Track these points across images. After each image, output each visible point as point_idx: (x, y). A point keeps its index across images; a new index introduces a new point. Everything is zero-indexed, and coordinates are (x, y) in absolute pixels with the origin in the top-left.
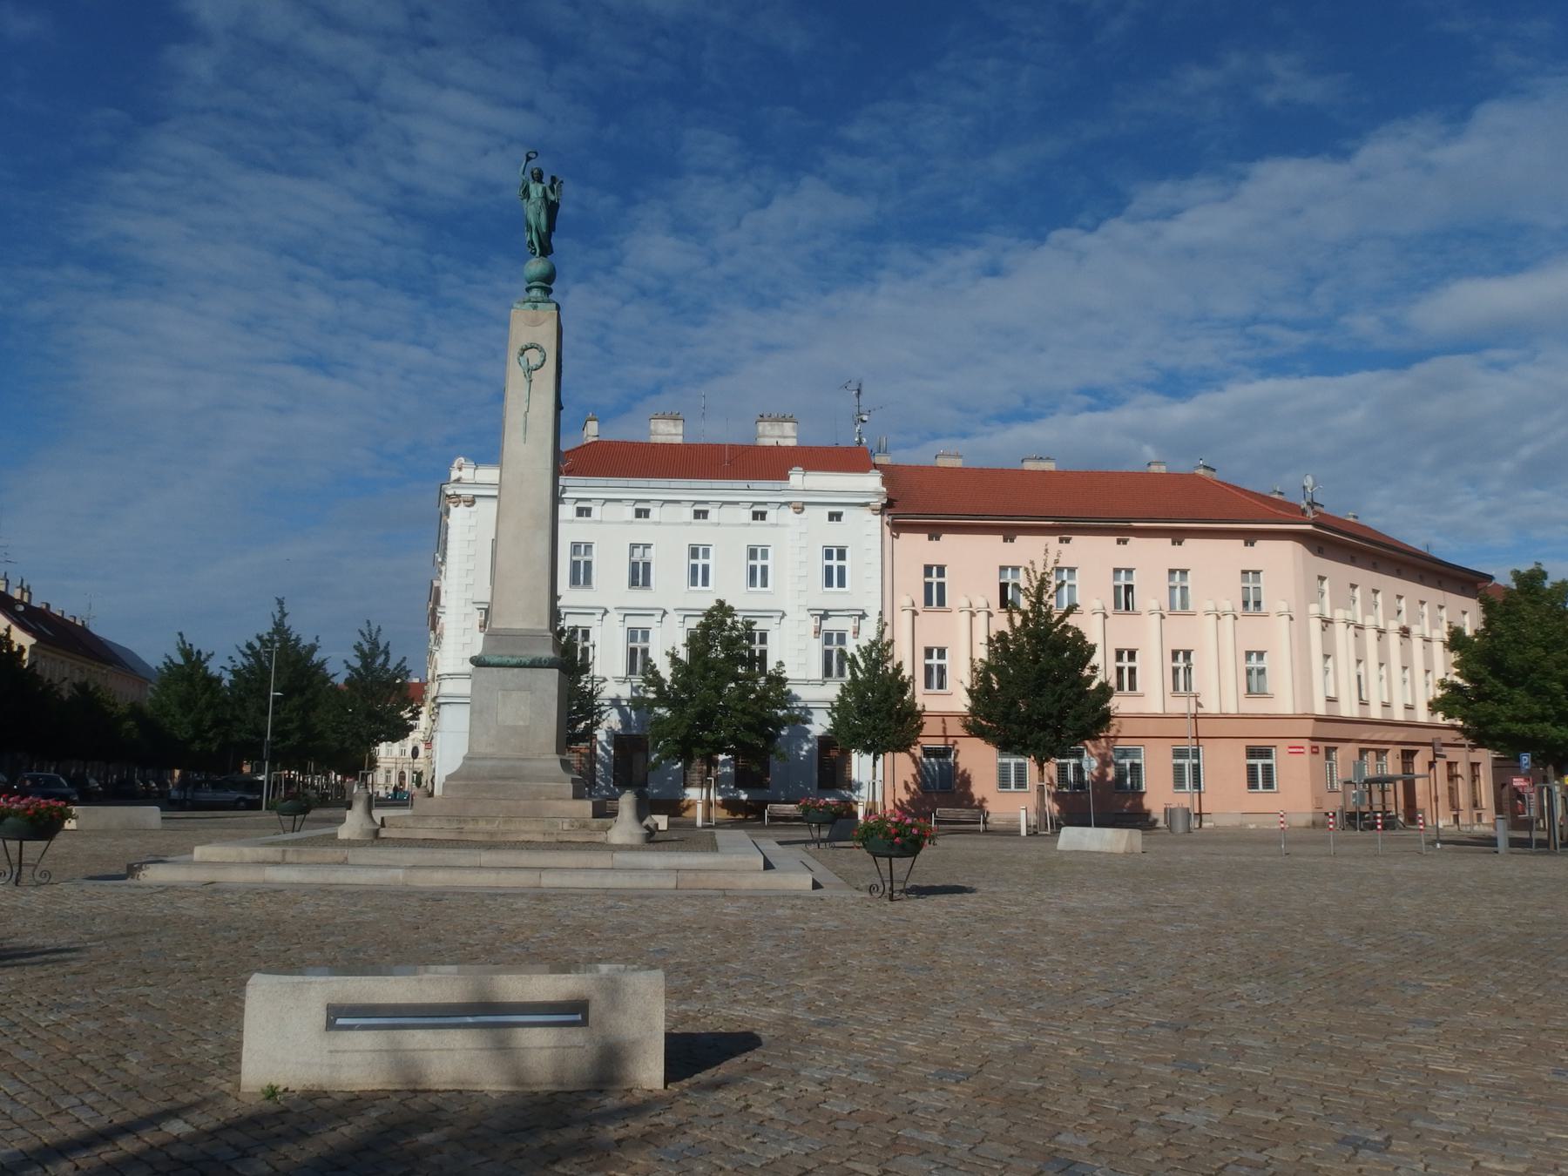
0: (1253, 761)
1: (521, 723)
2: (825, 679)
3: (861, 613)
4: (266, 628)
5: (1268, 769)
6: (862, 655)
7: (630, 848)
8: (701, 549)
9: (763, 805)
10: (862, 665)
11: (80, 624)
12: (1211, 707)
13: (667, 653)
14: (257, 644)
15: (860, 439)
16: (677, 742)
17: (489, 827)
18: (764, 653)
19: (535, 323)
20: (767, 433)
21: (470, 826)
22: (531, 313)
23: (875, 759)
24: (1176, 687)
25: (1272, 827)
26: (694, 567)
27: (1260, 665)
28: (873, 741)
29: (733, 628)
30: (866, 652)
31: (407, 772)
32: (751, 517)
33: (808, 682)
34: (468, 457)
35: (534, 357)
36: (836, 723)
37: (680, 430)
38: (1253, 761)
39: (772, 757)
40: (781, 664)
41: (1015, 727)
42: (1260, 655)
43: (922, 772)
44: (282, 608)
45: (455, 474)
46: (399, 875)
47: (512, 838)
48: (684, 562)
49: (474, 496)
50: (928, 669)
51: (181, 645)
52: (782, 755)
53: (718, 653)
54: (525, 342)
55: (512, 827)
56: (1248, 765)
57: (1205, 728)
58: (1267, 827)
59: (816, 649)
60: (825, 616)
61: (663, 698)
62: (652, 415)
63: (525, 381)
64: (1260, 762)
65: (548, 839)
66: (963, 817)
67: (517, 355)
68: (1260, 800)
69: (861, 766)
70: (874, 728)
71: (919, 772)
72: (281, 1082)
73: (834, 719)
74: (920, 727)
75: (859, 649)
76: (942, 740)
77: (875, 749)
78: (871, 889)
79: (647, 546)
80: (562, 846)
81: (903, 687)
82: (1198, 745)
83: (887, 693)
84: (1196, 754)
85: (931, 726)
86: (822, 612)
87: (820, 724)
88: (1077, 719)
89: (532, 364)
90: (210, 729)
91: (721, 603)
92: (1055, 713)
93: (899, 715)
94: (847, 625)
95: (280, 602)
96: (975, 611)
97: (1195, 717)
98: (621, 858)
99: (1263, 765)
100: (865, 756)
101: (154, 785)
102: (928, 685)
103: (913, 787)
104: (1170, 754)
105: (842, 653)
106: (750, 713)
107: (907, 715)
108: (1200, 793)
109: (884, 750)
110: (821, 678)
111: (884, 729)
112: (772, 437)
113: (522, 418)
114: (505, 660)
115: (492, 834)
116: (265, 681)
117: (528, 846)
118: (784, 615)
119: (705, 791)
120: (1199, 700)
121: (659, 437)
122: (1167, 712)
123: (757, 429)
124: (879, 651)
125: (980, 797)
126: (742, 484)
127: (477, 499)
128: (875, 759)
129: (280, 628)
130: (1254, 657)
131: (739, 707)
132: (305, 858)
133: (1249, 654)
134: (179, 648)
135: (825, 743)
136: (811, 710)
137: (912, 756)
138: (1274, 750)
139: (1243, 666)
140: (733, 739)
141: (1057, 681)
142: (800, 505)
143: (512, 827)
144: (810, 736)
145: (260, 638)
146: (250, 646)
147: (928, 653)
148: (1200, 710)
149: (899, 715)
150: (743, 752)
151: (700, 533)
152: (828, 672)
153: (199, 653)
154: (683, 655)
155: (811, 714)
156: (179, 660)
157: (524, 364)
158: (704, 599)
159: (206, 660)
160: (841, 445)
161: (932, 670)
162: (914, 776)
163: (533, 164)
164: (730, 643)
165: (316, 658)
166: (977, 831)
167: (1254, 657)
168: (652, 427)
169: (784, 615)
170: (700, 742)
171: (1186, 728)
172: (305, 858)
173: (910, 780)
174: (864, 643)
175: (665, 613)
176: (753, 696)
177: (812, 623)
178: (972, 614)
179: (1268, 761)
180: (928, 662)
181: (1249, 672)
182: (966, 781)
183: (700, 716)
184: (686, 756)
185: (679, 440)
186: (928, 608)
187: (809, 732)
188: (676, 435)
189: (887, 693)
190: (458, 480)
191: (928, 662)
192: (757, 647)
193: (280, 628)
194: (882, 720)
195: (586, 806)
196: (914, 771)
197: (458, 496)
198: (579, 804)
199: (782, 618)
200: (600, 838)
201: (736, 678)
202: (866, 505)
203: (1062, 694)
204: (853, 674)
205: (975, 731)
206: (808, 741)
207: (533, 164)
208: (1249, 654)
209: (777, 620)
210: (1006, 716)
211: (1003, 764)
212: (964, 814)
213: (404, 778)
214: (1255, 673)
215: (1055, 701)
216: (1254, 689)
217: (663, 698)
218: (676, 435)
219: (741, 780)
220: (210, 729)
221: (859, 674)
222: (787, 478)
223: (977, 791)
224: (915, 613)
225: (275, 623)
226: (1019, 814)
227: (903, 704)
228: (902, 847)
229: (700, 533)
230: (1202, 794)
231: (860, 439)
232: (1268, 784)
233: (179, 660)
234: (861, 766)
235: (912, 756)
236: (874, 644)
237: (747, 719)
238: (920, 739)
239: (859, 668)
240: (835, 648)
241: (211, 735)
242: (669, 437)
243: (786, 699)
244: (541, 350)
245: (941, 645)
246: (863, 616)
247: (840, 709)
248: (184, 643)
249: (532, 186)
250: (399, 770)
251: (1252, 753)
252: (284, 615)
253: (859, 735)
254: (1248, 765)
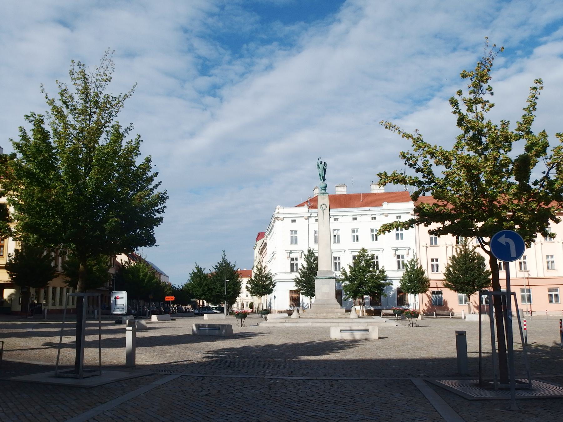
0: (551, 293)
1: (327, 292)
2: (398, 270)
3: (409, 248)
4: (221, 260)
5: (557, 296)
6: (409, 263)
7: (355, 318)
8: (355, 230)
9: (380, 310)
10: (409, 266)
11: (139, 256)
12: (533, 275)
13: (348, 265)
14: (218, 265)
15: (406, 188)
16: (353, 292)
17: (323, 315)
18: (377, 262)
19: (324, 199)
20: (374, 189)
21: (318, 315)
22: (323, 196)
23: (415, 295)
24: (521, 269)
25: (559, 316)
26: (354, 236)
27: (552, 260)
28: (414, 290)
29: (368, 256)
30: (411, 263)
31: (244, 303)
32: (371, 219)
33: (393, 271)
34: (281, 205)
35: (324, 207)
36: (402, 285)
37: (345, 189)
38: (551, 293)
39: (382, 296)
40: (383, 267)
41: (459, 285)
42: (552, 256)
43: (431, 301)
44: (224, 253)
45: (277, 211)
46: (310, 324)
47: (329, 317)
48: (350, 234)
49: (284, 217)
50: (433, 266)
51: (196, 266)
52: (385, 295)
53: (363, 264)
54: (322, 203)
55: (328, 315)
56: (549, 295)
57: (531, 282)
58: (557, 316)
59: (395, 260)
60: (397, 249)
61: (347, 278)
62: (336, 186)
63: (322, 213)
64: (553, 293)
65: (336, 317)
66: (445, 314)
67: (320, 207)
68: (554, 306)
69: (411, 298)
70: (414, 286)
71: (430, 300)
72: (481, 255)
73: (401, 284)
74: (429, 285)
75: (408, 261)
76: (436, 289)
77: (415, 292)
78: (408, 325)
79: (338, 230)
80: (340, 318)
81: (423, 273)
82: (529, 288)
83: (418, 275)
84: (529, 291)
85: (433, 284)
86: (396, 249)
87: (396, 285)
88: (479, 282)
89: (324, 209)
90: (207, 291)
91: (363, 249)
92: (472, 280)
93: (422, 282)
94: (403, 252)
95: (224, 252)
96: (448, 246)
97: (528, 279)
98: (354, 320)
99: (554, 294)
100: (412, 295)
101: (162, 309)
102: (433, 271)
103: (428, 305)
104: (520, 291)
105: (403, 263)
106: (374, 283)
107: (425, 282)
108: (531, 304)
109: (418, 292)
110: (396, 269)
111: (417, 286)
112: (376, 190)
113: (322, 221)
114: (322, 278)
115: (324, 316)
116: (223, 276)
117: (333, 318)
118: (383, 250)
119: (361, 306)
120: (529, 273)
121: (339, 192)
122: (518, 277)
123: (371, 188)
124: (413, 263)
125: (451, 308)
126: (367, 208)
127: (284, 218)
128: (415, 295)
129: (224, 259)
130: (550, 257)
131: (371, 281)
132: (289, 321)
133: (548, 256)
134: (196, 267)
135: (399, 290)
136: (392, 280)
137: (427, 295)
138: (558, 289)
139: (545, 261)
140: (370, 291)
141: (472, 270)
142: (387, 214)
143: (328, 315)
144: (393, 289)
145: (218, 263)
146: (217, 266)
147: (432, 260)
148: (529, 276)
149: (422, 282)
150: (372, 294)
151: (355, 225)
152: (399, 268)
153: (201, 268)
154: (352, 265)
155: (392, 282)
156: (196, 271)
157: (322, 209)
158: (358, 246)
159: (203, 270)
160: (399, 191)
161: (434, 266)
162: (428, 301)
163: (320, 160)
164: (367, 261)
165: (235, 269)
166: (449, 318)
167: (550, 257)
168: (336, 189)
169: (383, 250)
170: (359, 292)
171: (525, 282)
172: (289, 321)
173: (427, 303)
174: (410, 260)
175: (345, 251)
176: (375, 277)
177: (393, 252)
178: (447, 247)
179: (556, 293)
180: (433, 263)
181: (548, 262)
182: (446, 303)
183: (359, 284)
184: (355, 297)
185: (345, 193)
186: (432, 245)
187: (392, 288)
188: (344, 191)
189: (418, 275)
190: (278, 213)
191: (433, 263)
192: (375, 260)
193: (224, 259)
194: (416, 284)
195: (343, 310)
196: (428, 300)
197: (279, 218)
198: (342, 309)
199: (383, 251)
200: (348, 316)
201: (370, 272)
202: (409, 213)
203: (473, 275)
204: (407, 269)
205: (446, 286)
206: (392, 291)
207: (320, 160)
208: (548, 256)
209: (381, 251)
210: (456, 282)
211: (460, 296)
212: (445, 312)
213: (243, 305)
214: (550, 263)
215: (471, 277)
216: (550, 268)
217: (347, 278)
218: (344, 191)
219: (372, 303)
220: (207, 291)
221: (408, 269)
222: (382, 206)
223: (450, 306)
224: (427, 247)
225: (223, 258)
226: (461, 312)
227: (423, 278)
228: (414, 316)
229: (355, 225)
230: (532, 305)
231: (406, 188)
232: (557, 301)
233: (196, 271)
234: (411, 298)
235: (427, 295)
236: (413, 260)
237: (374, 284)
238: (429, 289)
239: (408, 267)
240: (401, 260)
241: (207, 293)
242: (342, 192)
243: (385, 278)
244: (326, 205)
245: (437, 257)
246: (409, 249)
247: (403, 280)
248: (197, 266)
249: (320, 165)
250: (241, 302)
251: (550, 290)
252: (225, 256)
253: (409, 288)
254: (549, 295)
